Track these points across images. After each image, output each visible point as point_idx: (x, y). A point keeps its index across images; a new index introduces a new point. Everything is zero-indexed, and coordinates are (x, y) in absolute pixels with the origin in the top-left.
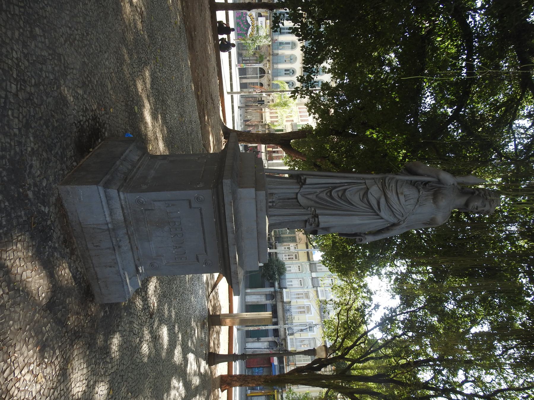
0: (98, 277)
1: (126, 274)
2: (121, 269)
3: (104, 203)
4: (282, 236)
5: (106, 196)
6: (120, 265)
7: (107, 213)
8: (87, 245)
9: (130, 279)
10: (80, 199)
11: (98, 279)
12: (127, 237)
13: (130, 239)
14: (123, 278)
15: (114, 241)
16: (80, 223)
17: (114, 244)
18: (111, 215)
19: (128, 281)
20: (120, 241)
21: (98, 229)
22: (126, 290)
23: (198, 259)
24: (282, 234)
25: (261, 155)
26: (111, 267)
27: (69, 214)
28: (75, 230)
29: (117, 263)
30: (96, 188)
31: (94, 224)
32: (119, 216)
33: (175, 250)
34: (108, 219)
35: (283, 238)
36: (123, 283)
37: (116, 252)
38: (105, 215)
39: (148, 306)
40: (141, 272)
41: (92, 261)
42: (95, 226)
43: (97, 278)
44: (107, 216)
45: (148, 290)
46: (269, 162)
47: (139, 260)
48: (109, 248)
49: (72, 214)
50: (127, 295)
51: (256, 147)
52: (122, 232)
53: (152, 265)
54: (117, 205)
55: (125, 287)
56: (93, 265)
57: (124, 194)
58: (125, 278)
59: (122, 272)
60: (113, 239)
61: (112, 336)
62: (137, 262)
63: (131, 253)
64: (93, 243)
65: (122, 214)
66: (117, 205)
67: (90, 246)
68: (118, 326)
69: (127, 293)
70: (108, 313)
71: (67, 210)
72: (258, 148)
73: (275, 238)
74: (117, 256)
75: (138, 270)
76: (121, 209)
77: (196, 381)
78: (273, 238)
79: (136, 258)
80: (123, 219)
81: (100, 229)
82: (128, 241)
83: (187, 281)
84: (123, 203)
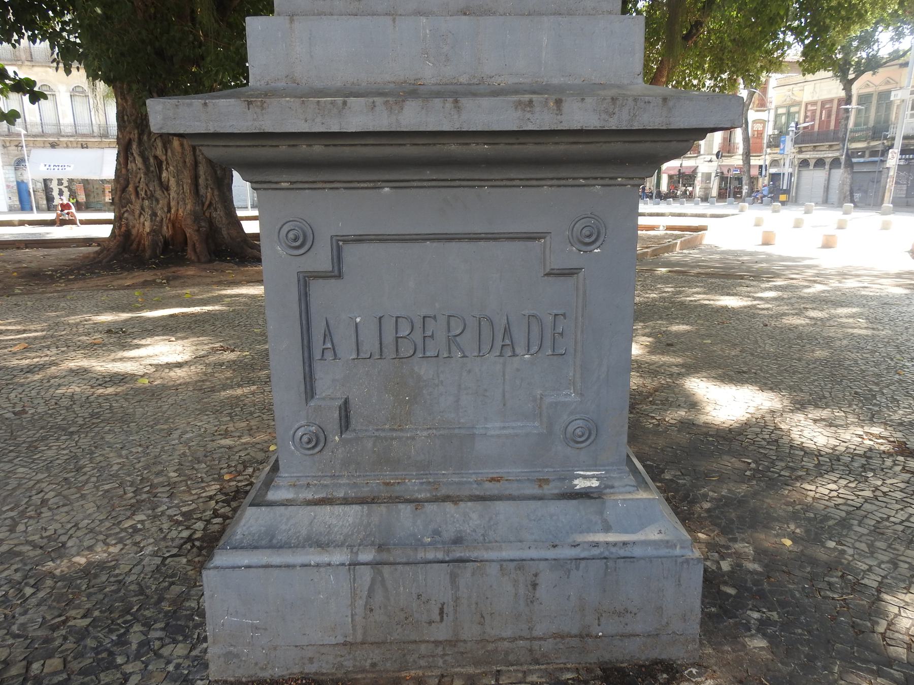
0: (575, 631)
1: (580, 538)
2: (551, 554)
3: (276, 558)
4: (871, 123)
5: (254, 547)
6: (533, 553)
7: (314, 557)
8: (437, 643)
9: (607, 529)
10: (256, 628)
11: (584, 635)
12: (430, 508)
13: (446, 499)
14: (596, 552)
15: (431, 555)
16: (345, 644)
17: (440, 556)
18: (322, 545)
19: (611, 537)
20: (437, 532)
21: (369, 596)
22: (650, 551)
23: (570, 273)
24: (866, 123)
25: (687, 168)
26: (535, 585)
27: (311, 669)
28: (374, 665)
29: (520, 564)
30: (211, 573)
31: (352, 605)
32: (342, 519)
33: (518, 351)
34: (339, 557)
35: (877, 122)
36: (612, 561)
37: (474, 555)
38: (318, 565)
39: (864, 456)
40: (595, 483)
41: (504, 639)
42: (361, 603)
43: (581, 636)
44: (326, 558)
45: (809, 444)
46: (702, 152)
47: (542, 482)
48: (453, 577)
49: (311, 660)
50: (678, 551)
51: (671, 177)
52: (405, 519)
53: (574, 440)
54: (302, 520)
55: (637, 552)
56: (521, 638)
57: (278, 487)
58: (596, 545)
59: (568, 553)
60: (421, 555)
61: (881, 628)
62: (551, 489)
63: (500, 506)
64: (430, 623)
65: (339, 509)
66: (302, 520)
67: (442, 632)
68: (857, 587)
69: (663, 552)
70: (775, 616)
71: (296, 670)
72: (672, 173)
73: (874, 138)
74: (487, 555)
75: (585, 495)
76: (317, 508)
77: (27, 409)
78: (873, 143)
79: (535, 490)
80: (357, 508)
81: (371, 590)
82: (449, 507)
83: (869, 332)
84: (310, 496)
